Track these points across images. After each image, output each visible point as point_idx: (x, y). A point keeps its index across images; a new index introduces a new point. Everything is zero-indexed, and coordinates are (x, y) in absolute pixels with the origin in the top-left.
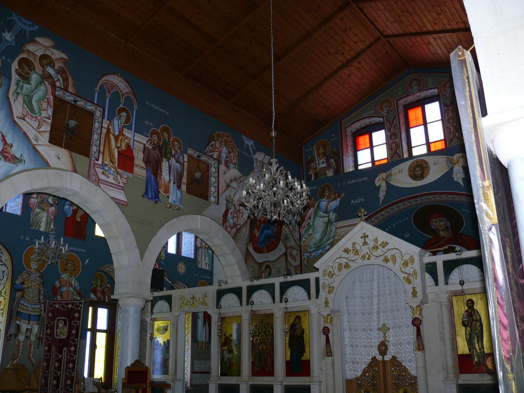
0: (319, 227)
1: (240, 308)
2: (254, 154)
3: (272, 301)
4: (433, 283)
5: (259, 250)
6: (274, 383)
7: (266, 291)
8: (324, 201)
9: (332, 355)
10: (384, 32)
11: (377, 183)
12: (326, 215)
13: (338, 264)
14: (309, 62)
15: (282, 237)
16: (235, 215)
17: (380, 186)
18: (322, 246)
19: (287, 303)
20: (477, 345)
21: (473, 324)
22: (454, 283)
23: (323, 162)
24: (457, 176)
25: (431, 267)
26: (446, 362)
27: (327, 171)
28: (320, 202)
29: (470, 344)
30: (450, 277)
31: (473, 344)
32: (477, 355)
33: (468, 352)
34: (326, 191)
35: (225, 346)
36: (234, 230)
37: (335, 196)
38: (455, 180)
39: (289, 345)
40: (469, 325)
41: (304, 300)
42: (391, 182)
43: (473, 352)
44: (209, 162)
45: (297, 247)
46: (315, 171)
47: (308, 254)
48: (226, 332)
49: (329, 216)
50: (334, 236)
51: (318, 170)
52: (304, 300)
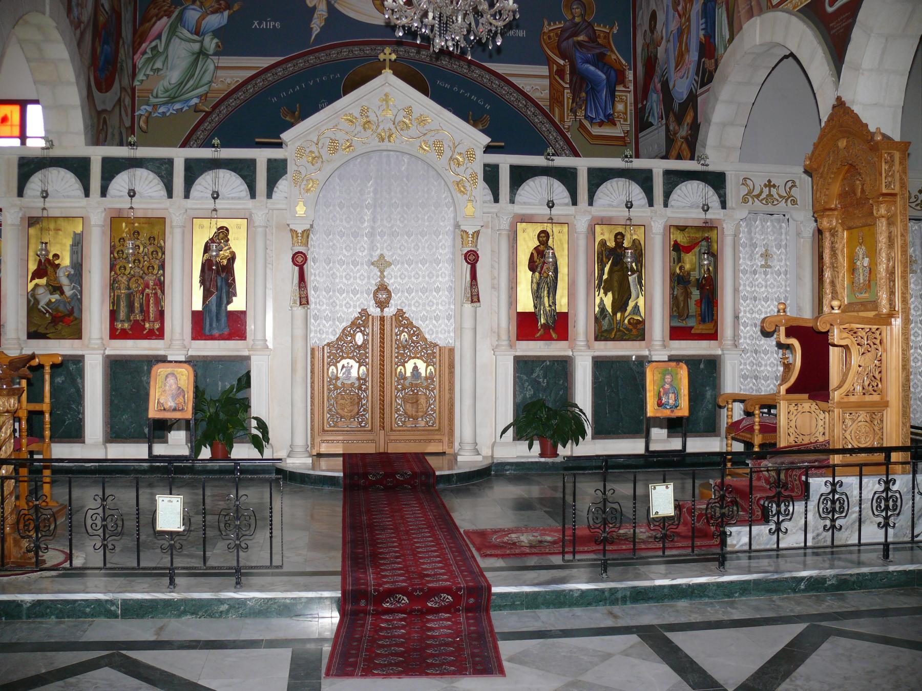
0: (178, 57)
1: (84, 201)
3: (164, 193)
4: (645, 201)
6: (170, 352)
9: (479, 301)
12: (195, 37)
13: (328, 140)
17: (314, 8)
20: (546, 299)
21: (545, 268)
25: (489, 171)
28: (185, 9)
31: (541, 298)
35: (40, 277)
40: (539, 269)
41: (239, 198)
42: (336, 5)
43: (540, 310)
45: (129, 91)
47: (149, 109)
49: (202, 42)
50: (210, 82)
52: (239, 198)
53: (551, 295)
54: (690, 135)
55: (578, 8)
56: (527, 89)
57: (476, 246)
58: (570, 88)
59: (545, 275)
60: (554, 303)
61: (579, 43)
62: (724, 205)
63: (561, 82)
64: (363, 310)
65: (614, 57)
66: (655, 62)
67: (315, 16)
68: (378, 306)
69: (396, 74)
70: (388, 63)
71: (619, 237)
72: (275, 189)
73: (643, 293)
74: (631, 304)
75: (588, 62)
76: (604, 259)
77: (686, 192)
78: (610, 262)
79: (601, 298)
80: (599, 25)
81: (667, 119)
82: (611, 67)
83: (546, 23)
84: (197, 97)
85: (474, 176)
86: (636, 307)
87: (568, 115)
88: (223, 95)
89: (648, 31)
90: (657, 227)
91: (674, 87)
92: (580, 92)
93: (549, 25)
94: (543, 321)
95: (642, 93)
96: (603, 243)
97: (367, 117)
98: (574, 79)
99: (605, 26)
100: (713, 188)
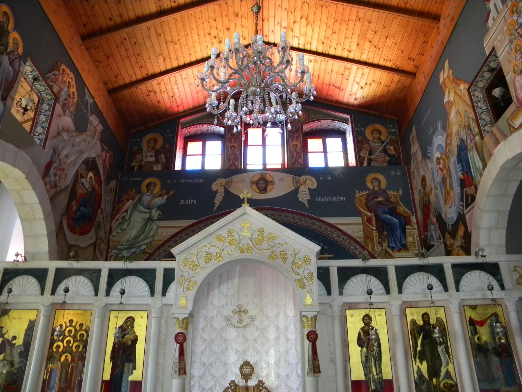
2: (91, 115)
3: (93, 293)
5: (73, 230)
7: (87, 278)
8: (147, 195)
10: (266, 36)
11: (214, 187)
12: (147, 210)
14: (187, 35)
15: (95, 223)
16: (58, 173)
17: (217, 191)
18: (136, 245)
19: (123, 296)
20: (374, 369)
22: (350, 294)
23: (151, 156)
24: (302, 196)
26: (337, 389)
27: (154, 166)
28: (143, 195)
29: (366, 367)
30: (345, 287)
31: (369, 368)
32: (374, 381)
33: (363, 378)
34: (152, 185)
36: (53, 191)
37: (162, 192)
38: (300, 199)
39: (111, 358)
41: (143, 296)
42: (229, 189)
44: (43, 95)
45: (106, 241)
46: (140, 163)
47: (117, 252)
48: (7, 331)
49: (150, 213)
50: (154, 236)
51: (143, 162)
52: (143, 296)
53: (377, 366)
54: (464, 243)
55: (375, 182)
56: (349, 232)
57: (315, 327)
58: (377, 229)
59: (371, 349)
60: (381, 372)
61: (379, 202)
62: (502, 288)
63: (371, 226)
64: (232, 381)
65: (402, 209)
66: (429, 205)
67: (217, 196)
68: (244, 378)
69: (251, 206)
70: (246, 200)
71: (425, 316)
72: (168, 289)
73: (452, 360)
74: (443, 371)
75: (386, 213)
76: (416, 335)
77: (471, 280)
78: (421, 337)
79: (418, 367)
80: (390, 190)
81: (444, 238)
82: (401, 215)
83: (357, 192)
84: (146, 245)
85: (311, 274)
86: (448, 373)
87: (377, 246)
88: (160, 243)
89: (422, 189)
90: (454, 308)
91: (446, 215)
92: (383, 231)
93: (359, 192)
94: (373, 387)
95: (424, 227)
96: (414, 322)
97: (233, 236)
98: (379, 224)
99: (394, 191)
100: (492, 275)
